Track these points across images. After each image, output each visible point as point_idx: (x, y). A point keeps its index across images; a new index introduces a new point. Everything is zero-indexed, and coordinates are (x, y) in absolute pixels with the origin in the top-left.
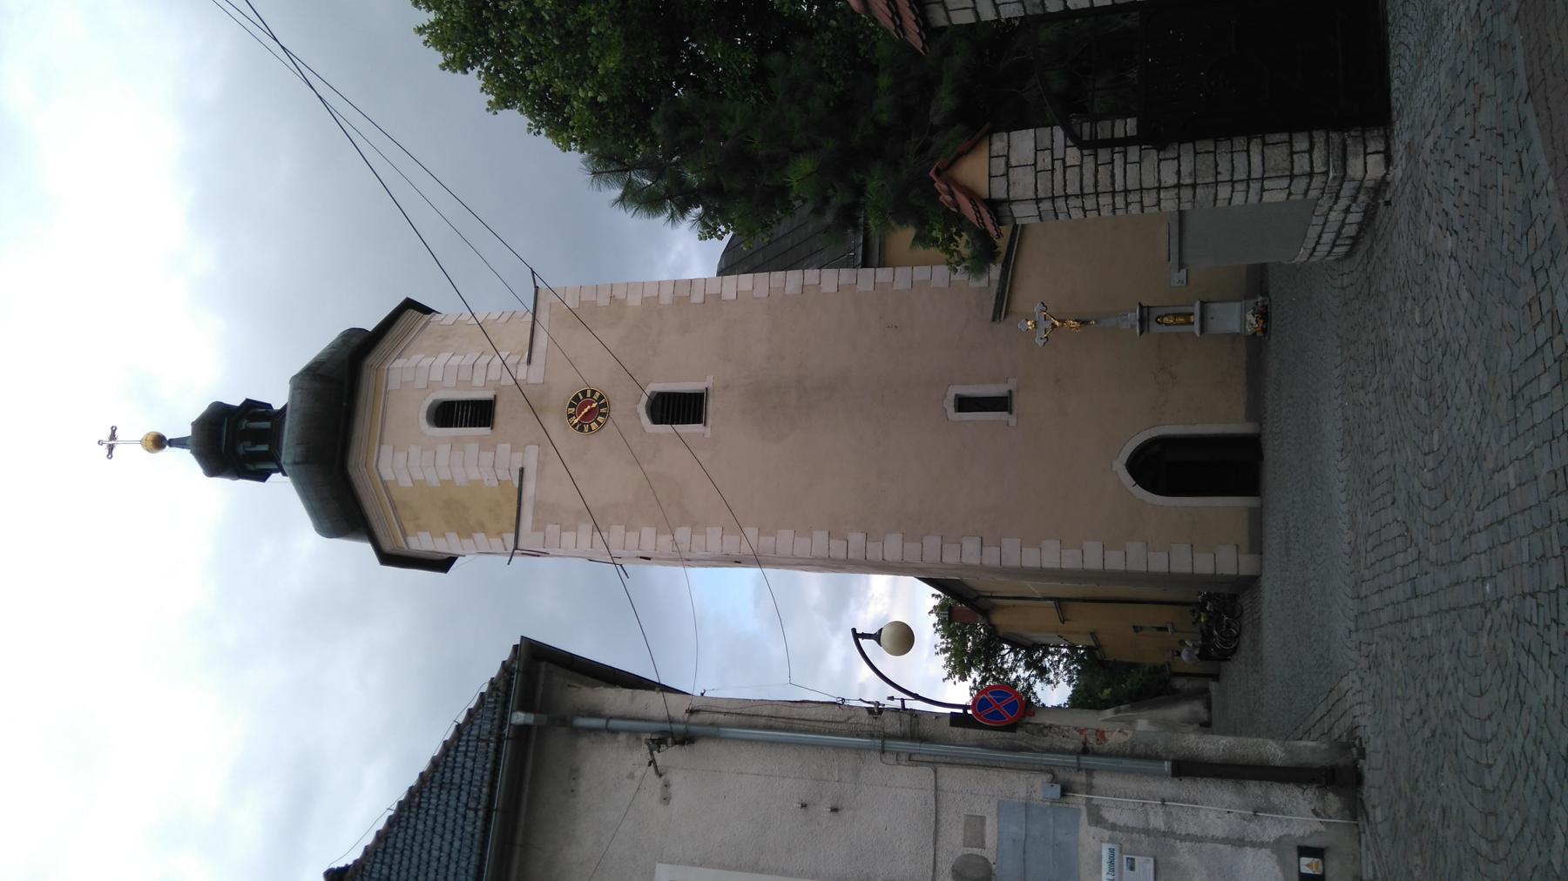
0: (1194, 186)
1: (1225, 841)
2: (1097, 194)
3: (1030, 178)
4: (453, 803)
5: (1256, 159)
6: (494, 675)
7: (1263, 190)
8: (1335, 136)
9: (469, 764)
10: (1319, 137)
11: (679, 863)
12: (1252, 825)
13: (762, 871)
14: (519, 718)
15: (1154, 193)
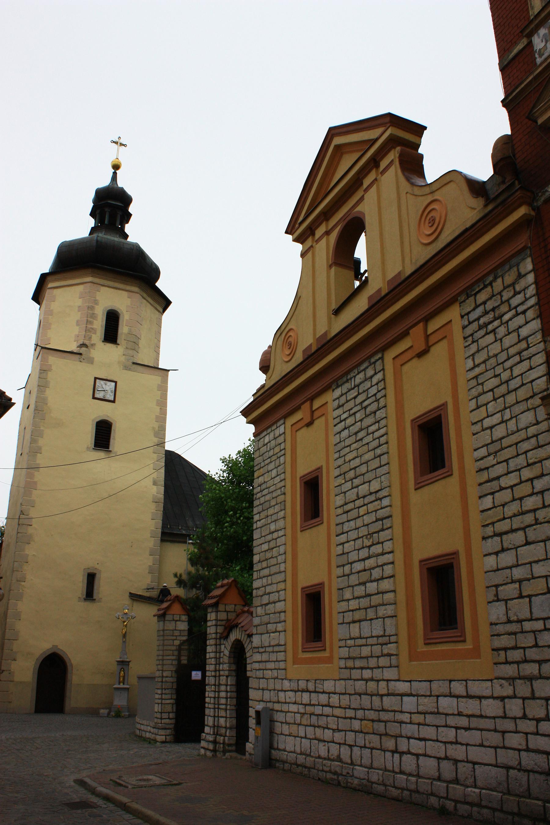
0: (162, 682)
2: (163, 650)
3: (171, 628)
5: (168, 701)
6: (6, 394)
7: (158, 704)
10: (173, 721)
15: (161, 669)
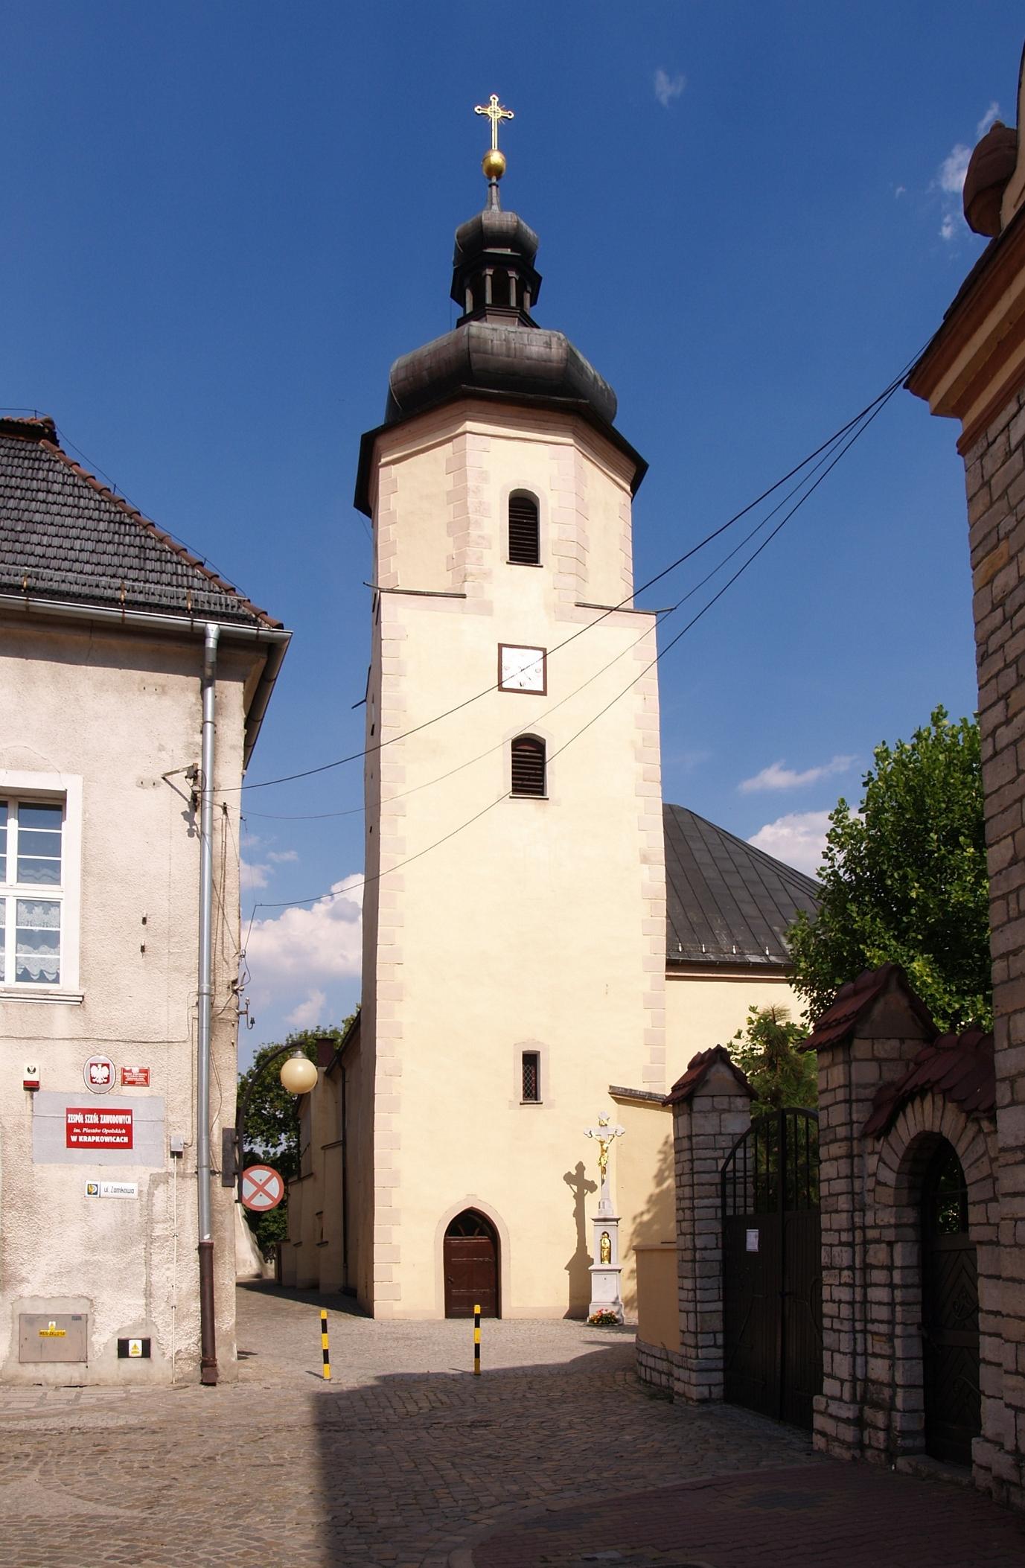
1: (149, 1284)
3: (710, 1130)
4: (127, 561)
7: (688, 1312)
8: (720, 1364)
9: (165, 578)
11: (85, 798)
12: (163, 1305)
13: (84, 880)
14: (213, 629)
